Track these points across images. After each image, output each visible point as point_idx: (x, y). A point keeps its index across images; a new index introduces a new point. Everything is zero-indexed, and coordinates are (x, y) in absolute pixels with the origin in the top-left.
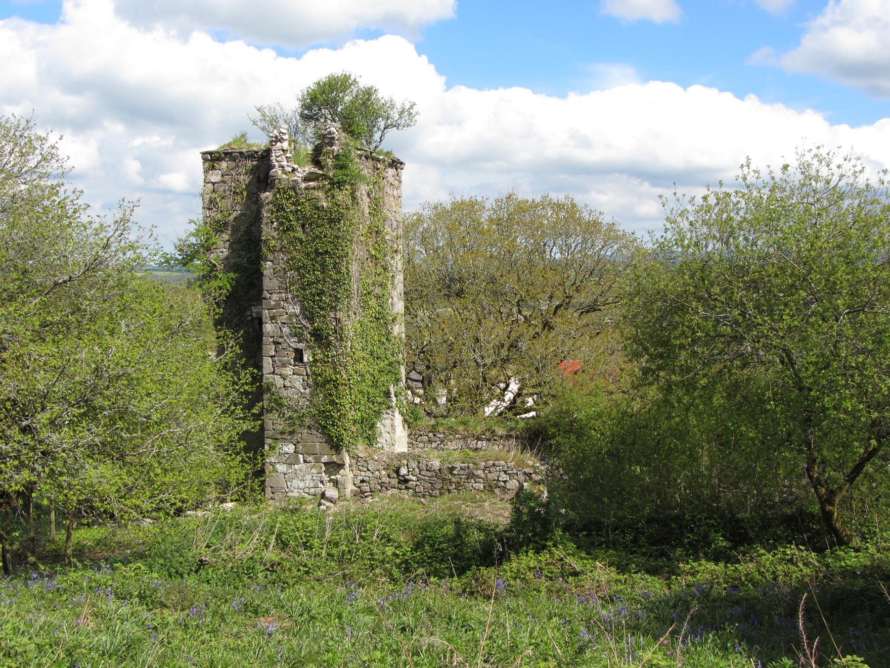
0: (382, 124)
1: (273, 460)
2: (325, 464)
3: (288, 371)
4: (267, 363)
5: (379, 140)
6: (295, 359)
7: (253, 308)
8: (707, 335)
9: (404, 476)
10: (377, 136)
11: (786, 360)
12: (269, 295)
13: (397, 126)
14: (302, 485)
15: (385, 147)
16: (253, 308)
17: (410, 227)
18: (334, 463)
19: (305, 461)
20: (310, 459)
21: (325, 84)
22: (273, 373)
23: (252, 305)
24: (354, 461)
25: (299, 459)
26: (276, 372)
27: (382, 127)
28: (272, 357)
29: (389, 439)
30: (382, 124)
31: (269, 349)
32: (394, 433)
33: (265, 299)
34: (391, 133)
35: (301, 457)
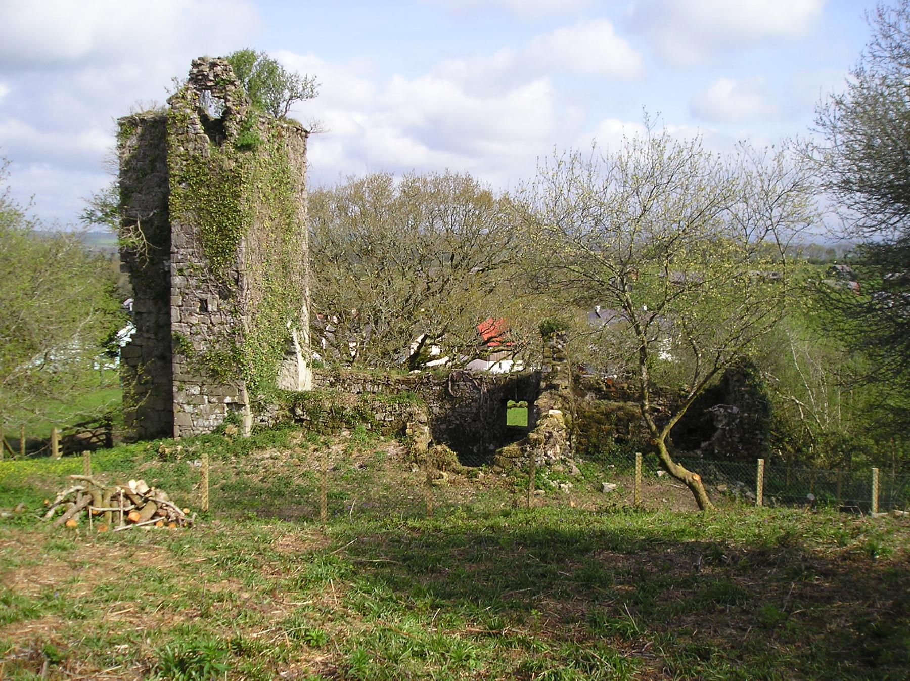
0: (287, 94)
1: (181, 401)
2: (228, 404)
3: (194, 319)
4: (175, 313)
5: (284, 110)
6: (201, 309)
7: (165, 262)
8: (875, 115)
9: (299, 416)
10: (283, 105)
11: (874, 229)
12: (176, 250)
13: (300, 97)
14: (206, 423)
15: (289, 115)
16: (165, 262)
17: (318, 203)
18: (235, 403)
19: (209, 402)
20: (214, 400)
21: (233, 57)
22: (180, 322)
23: (164, 260)
24: (825, 594)
25: (204, 400)
26: (183, 320)
27: (287, 97)
28: (179, 306)
29: (293, 383)
30: (287, 94)
31: (176, 299)
32: (298, 378)
33: (173, 253)
34: (296, 104)
35: (206, 397)
